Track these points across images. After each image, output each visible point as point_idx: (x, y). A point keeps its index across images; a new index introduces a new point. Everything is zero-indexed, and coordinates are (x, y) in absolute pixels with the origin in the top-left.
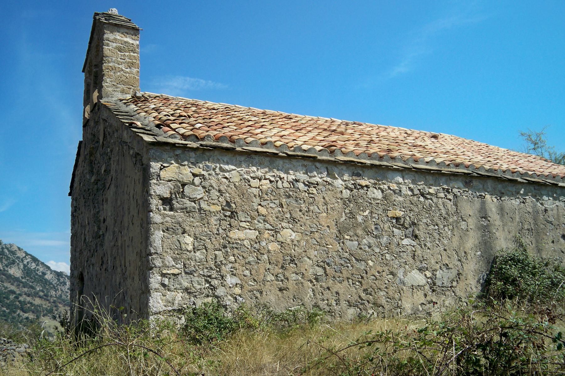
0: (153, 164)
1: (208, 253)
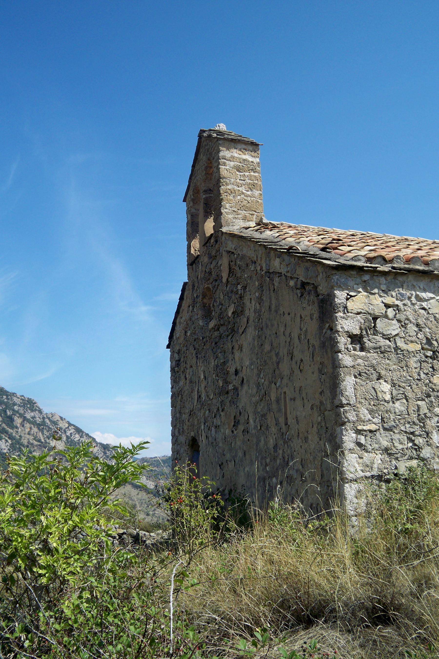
0: (337, 293)
1: (409, 404)
